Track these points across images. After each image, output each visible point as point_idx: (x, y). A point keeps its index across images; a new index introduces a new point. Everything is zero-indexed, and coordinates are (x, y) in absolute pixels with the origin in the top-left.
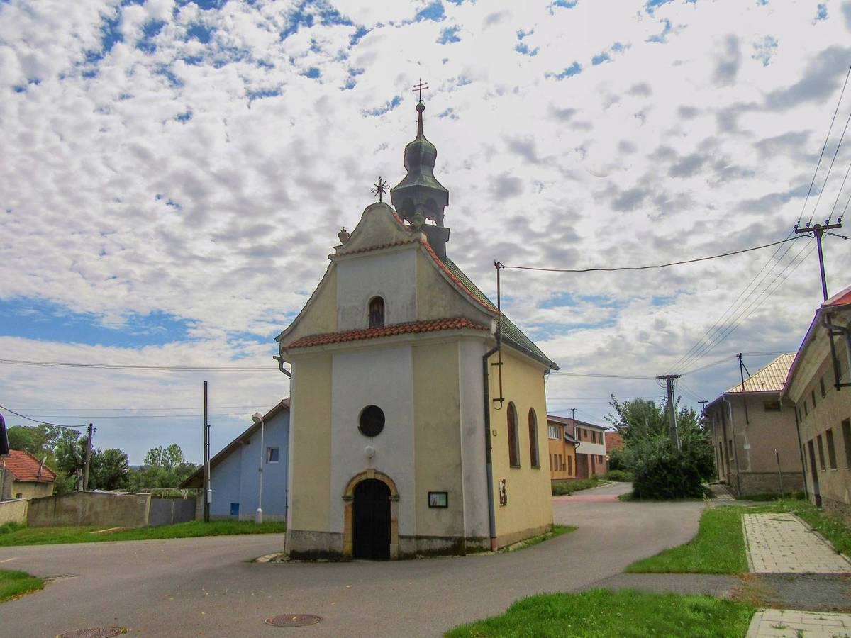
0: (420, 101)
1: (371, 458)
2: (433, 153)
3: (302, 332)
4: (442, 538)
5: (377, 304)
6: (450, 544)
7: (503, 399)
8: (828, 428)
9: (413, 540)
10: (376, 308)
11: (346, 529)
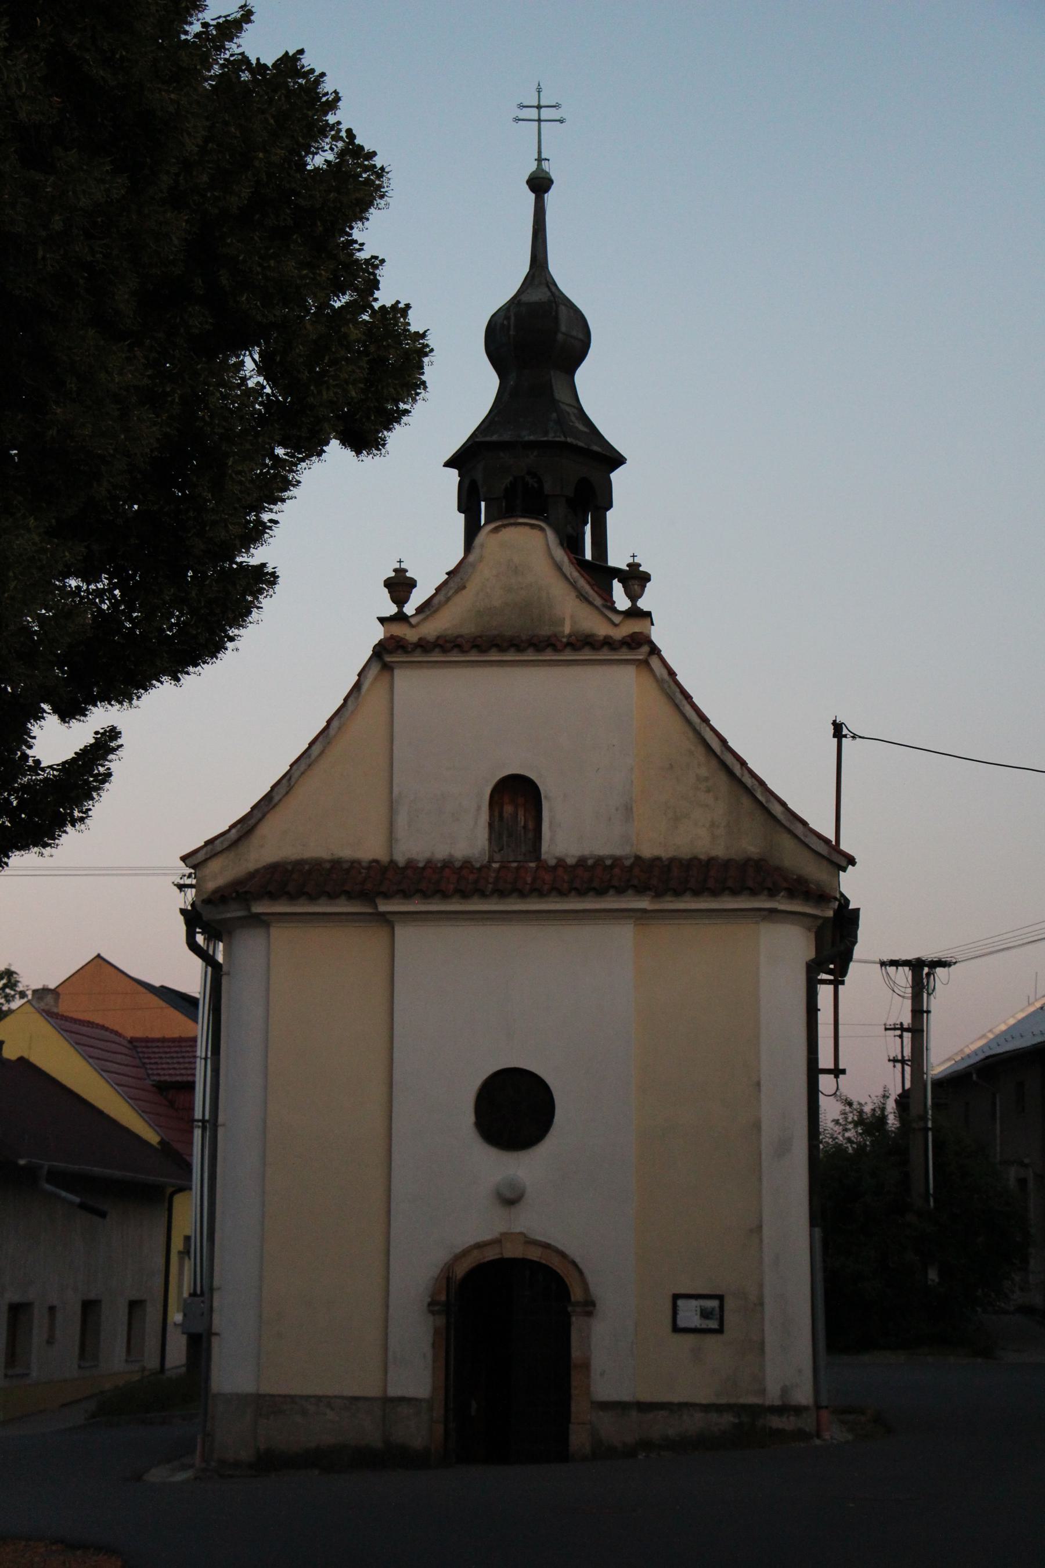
0: (540, 160)
1: (510, 1199)
2: (581, 336)
3: (270, 848)
4: (707, 1408)
5: (517, 798)
6: (728, 1420)
7: (843, 1072)
8: (92, 1296)
9: (634, 1413)
10: (508, 809)
11: (434, 1389)
